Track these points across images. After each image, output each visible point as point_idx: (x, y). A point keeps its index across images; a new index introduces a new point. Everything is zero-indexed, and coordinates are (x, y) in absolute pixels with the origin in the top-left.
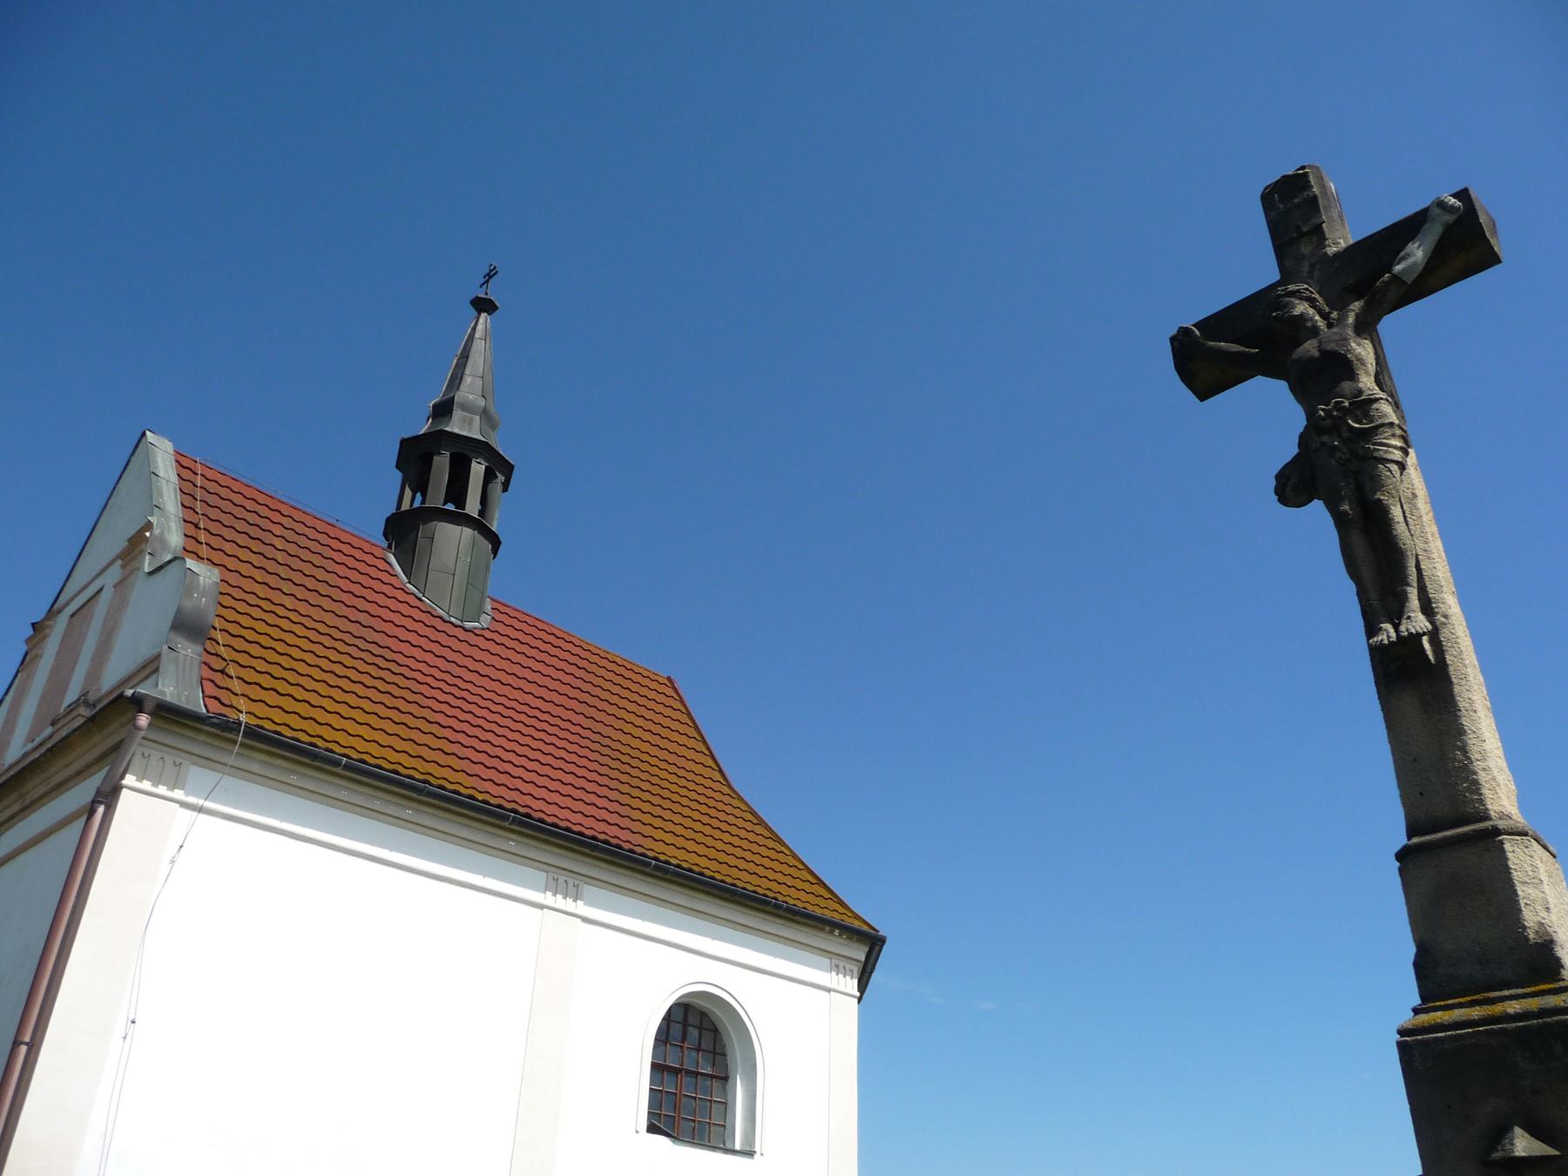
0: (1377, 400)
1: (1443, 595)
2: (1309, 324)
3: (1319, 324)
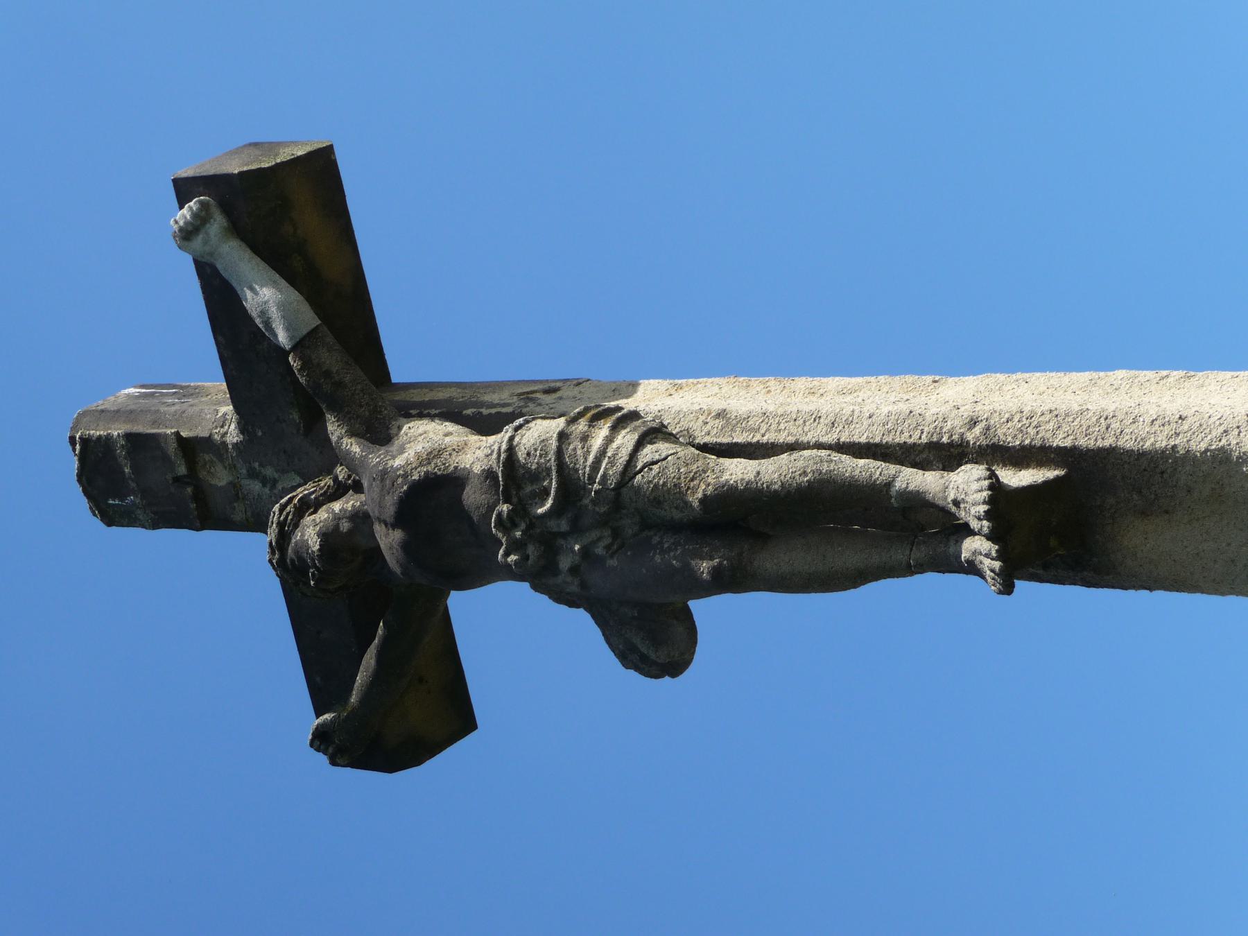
0: (511, 449)
1: (929, 418)
2: (345, 526)
3: (349, 506)
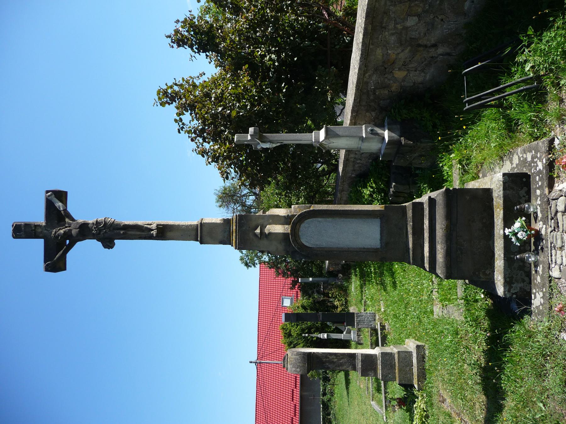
2: (67, 231)
